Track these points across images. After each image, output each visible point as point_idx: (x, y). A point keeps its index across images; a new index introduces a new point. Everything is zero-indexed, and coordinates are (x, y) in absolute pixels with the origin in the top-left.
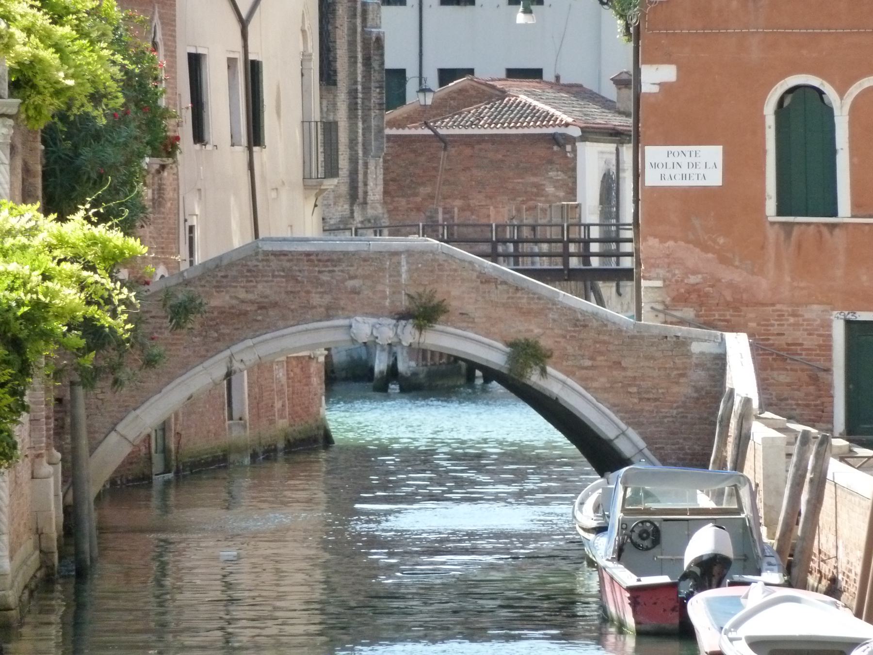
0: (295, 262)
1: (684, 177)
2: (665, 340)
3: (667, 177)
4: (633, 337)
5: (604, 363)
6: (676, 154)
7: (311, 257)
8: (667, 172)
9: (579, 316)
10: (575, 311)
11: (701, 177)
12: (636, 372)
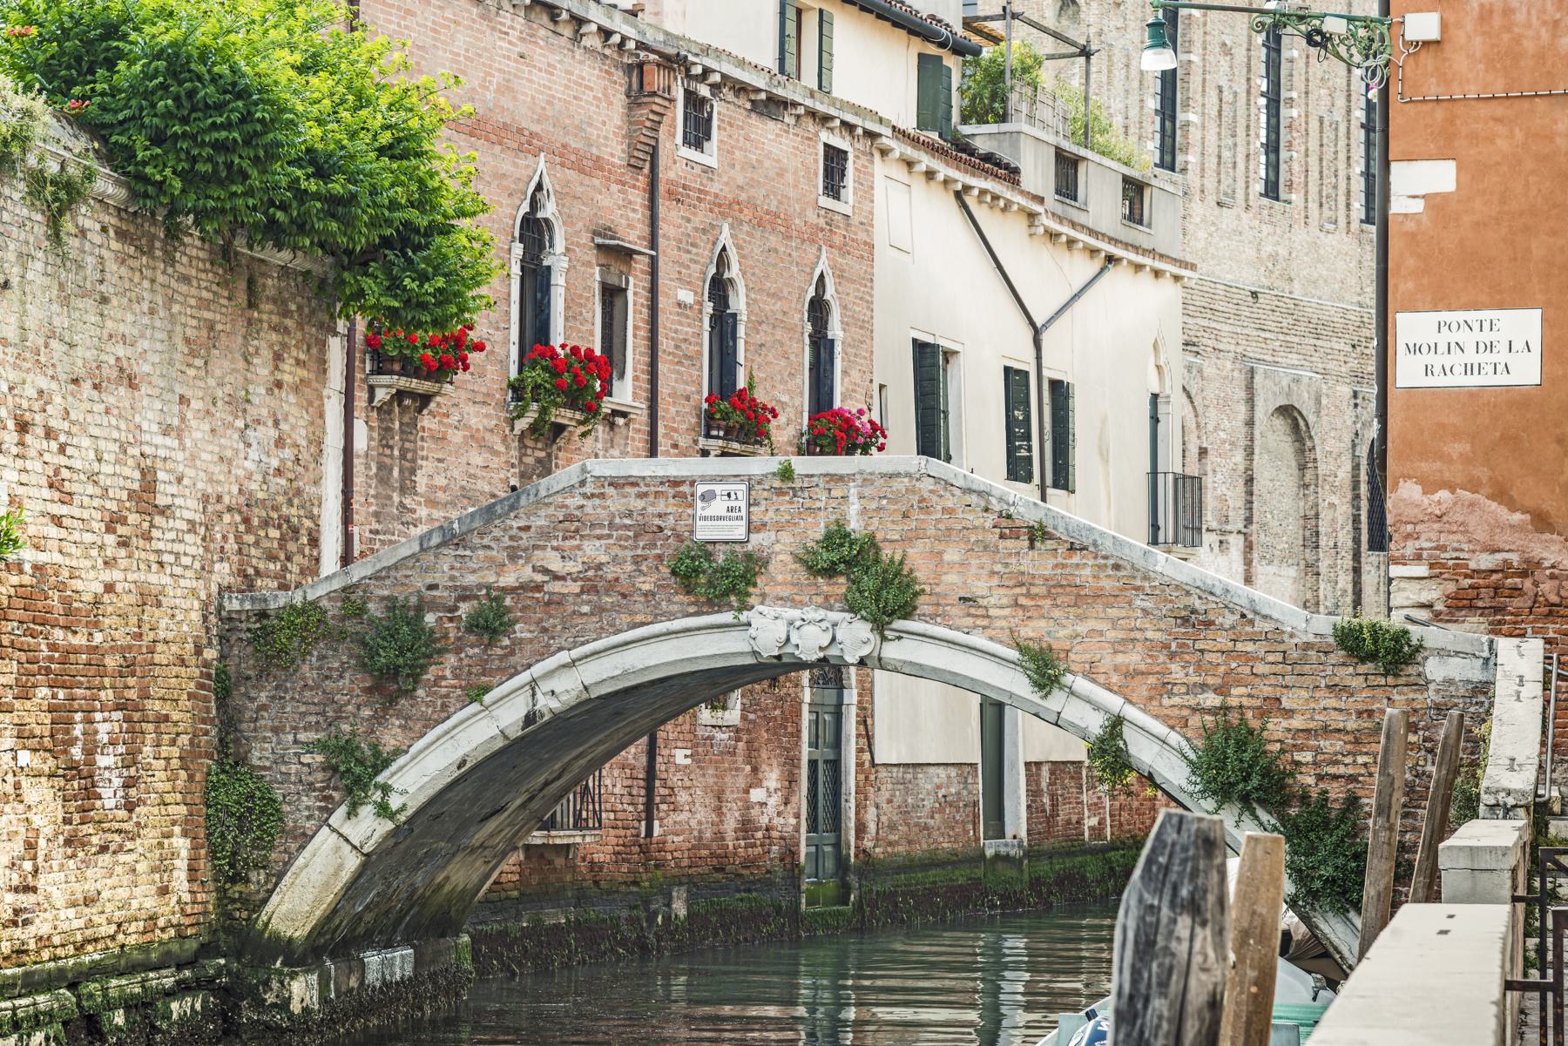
0: (651, 498)
1: (1468, 369)
3: (1437, 369)
4: (1308, 646)
8: (1437, 361)
11: (1500, 368)
12: (1312, 719)
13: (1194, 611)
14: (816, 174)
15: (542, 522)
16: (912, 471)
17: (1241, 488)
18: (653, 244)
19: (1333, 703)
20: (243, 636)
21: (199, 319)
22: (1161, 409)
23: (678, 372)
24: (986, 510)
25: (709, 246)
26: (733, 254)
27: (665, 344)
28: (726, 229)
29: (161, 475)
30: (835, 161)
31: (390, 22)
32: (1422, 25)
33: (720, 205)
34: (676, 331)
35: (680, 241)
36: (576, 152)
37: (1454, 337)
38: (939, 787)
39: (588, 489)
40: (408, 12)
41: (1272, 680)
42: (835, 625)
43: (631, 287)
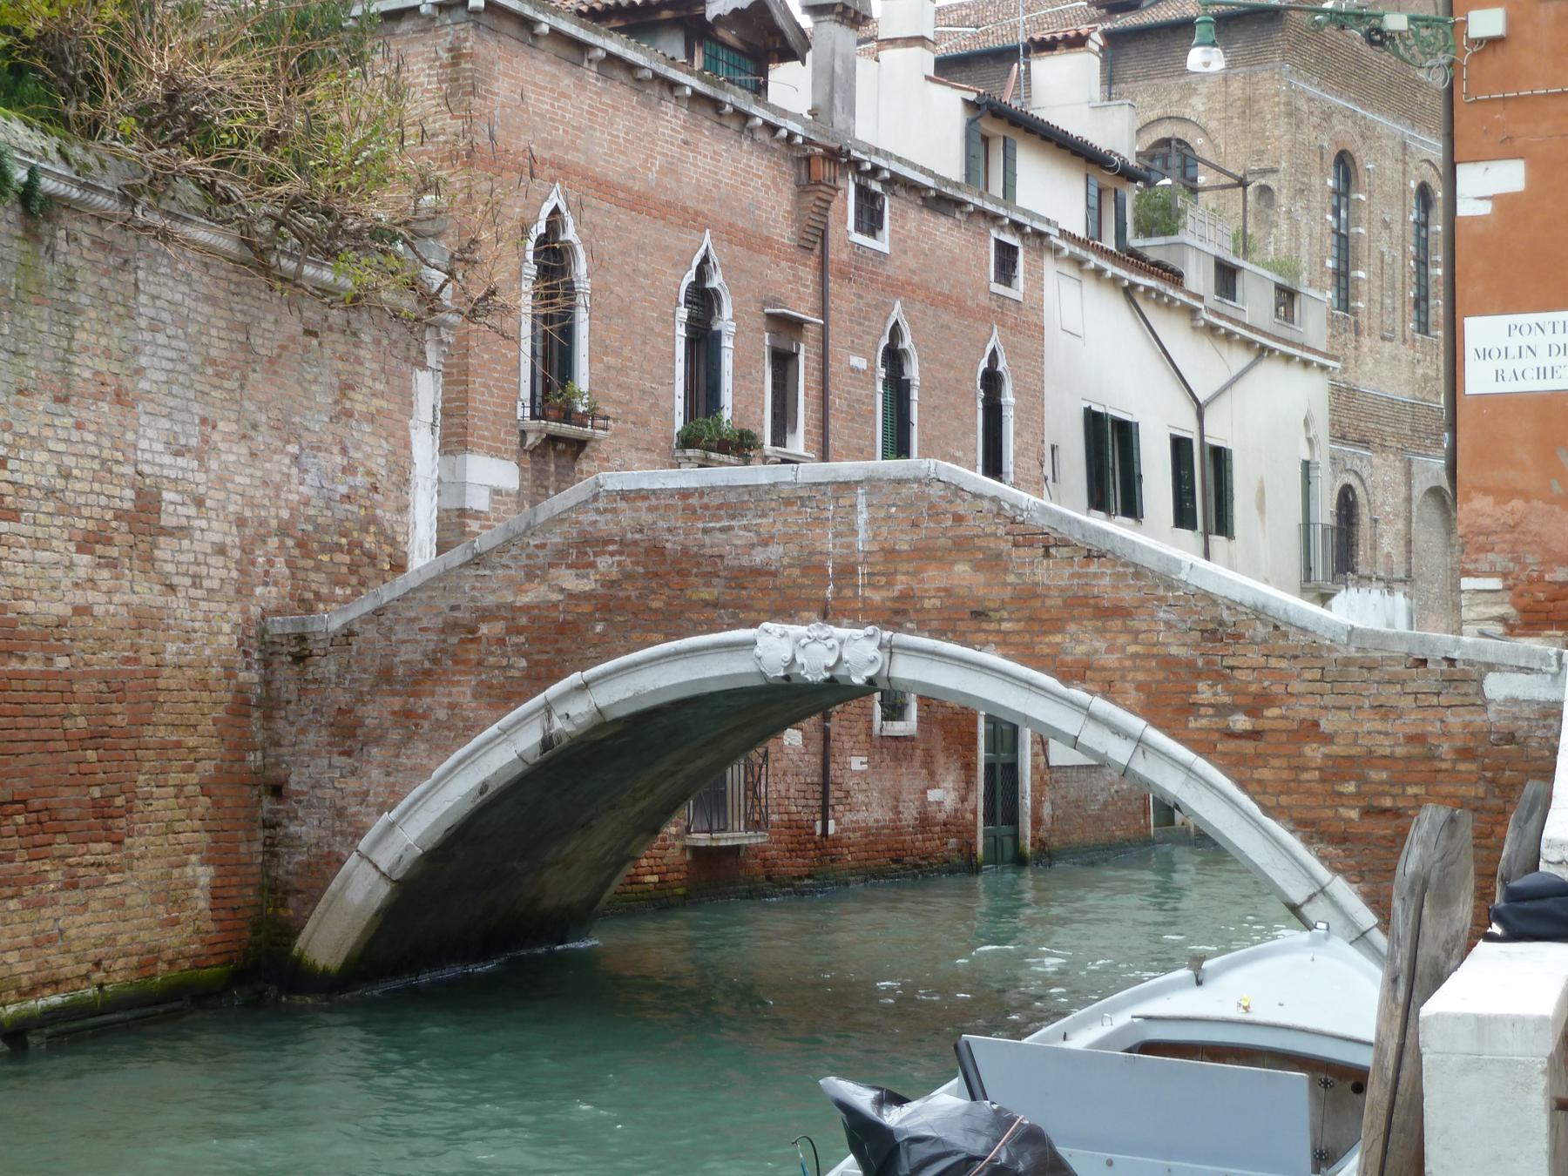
0: (662, 511)
1: (1542, 373)
2: (1421, 670)
4: (1348, 662)
5: (1281, 724)
6: (1525, 330)
7: (691, 501)
8: (1508, 366)
9: (1226, 615)
10: (1215, 603)
13: (1221, 623)
14: (988, 265)
15: (558, 540)
16: (921, 475)
17: (1402, 549)
18: (824, 313)
19: (1379, 726)
20: (284, 659)
21: (231, 341)
22: (1312, 474)
23: (852, 428)
24: (998, 514)
25: (881, 320)
26: (905, 328)
27: (836, 401)
28: (898, 305)
29: (168, 496)
30: (1006, 256)
31: (543, 102)
32: (1486, 23)
33: (892, 286)
34: (849, 393)
35: (853, 315)
36: (743, 230)
37: (1525, 340)
38: (1112, 784)
39: (601, 505)
40: (562, 95)
41: (1310, 700)
42: (842, 642)
43: (802, 351)
